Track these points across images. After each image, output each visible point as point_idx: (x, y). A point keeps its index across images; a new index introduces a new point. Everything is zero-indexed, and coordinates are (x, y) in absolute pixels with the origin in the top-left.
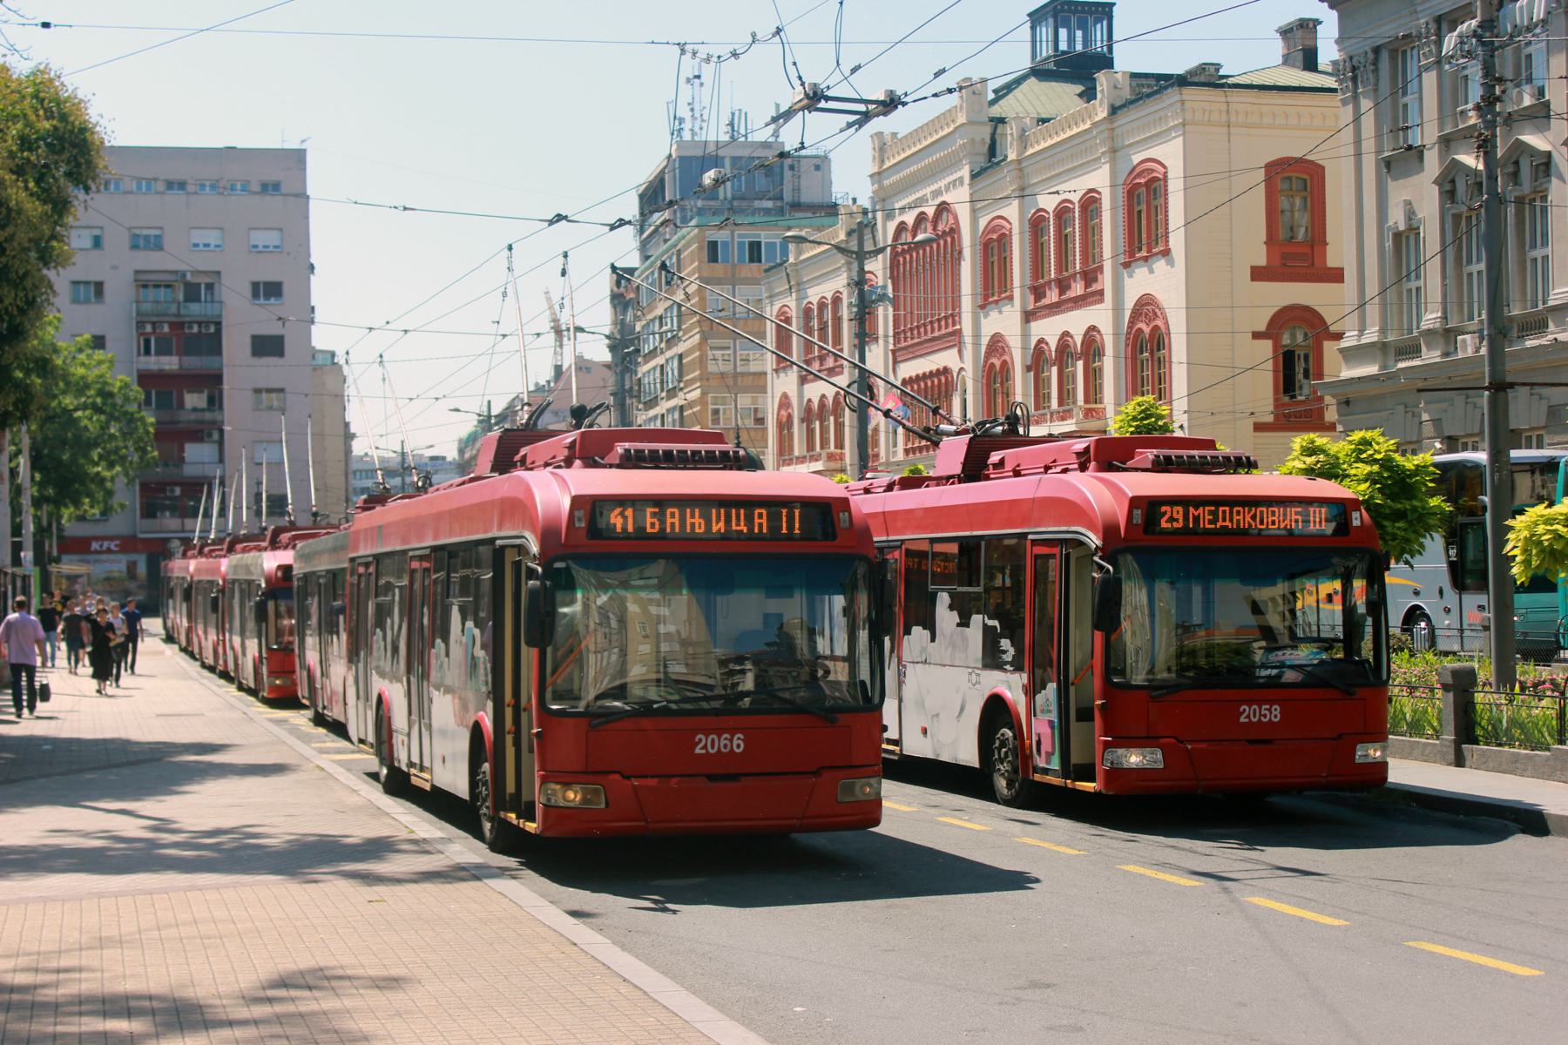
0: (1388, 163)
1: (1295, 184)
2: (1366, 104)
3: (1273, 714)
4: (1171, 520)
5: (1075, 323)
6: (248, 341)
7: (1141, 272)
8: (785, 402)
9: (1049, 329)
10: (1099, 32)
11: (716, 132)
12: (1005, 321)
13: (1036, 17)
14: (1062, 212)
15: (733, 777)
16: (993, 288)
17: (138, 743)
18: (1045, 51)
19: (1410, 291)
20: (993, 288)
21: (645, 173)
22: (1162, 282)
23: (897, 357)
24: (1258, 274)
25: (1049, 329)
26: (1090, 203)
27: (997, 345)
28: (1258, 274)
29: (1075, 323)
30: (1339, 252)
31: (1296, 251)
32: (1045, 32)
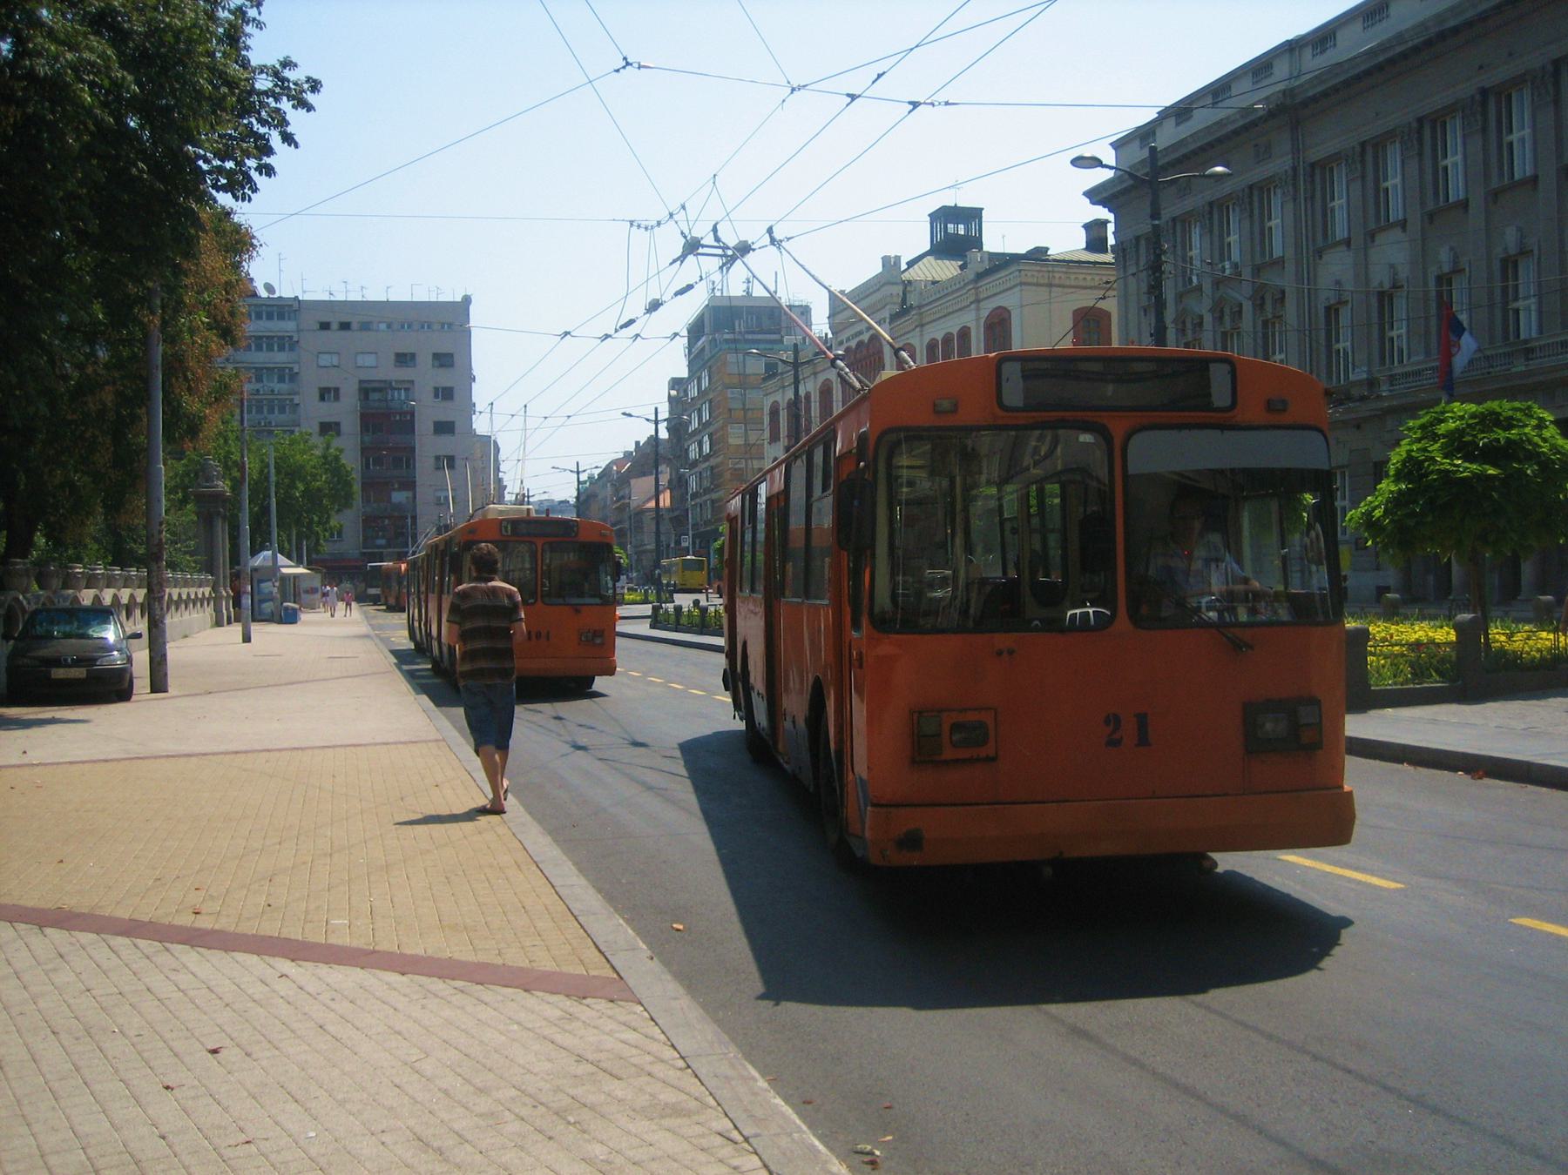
14: (948, 339)
26: (964, 333)
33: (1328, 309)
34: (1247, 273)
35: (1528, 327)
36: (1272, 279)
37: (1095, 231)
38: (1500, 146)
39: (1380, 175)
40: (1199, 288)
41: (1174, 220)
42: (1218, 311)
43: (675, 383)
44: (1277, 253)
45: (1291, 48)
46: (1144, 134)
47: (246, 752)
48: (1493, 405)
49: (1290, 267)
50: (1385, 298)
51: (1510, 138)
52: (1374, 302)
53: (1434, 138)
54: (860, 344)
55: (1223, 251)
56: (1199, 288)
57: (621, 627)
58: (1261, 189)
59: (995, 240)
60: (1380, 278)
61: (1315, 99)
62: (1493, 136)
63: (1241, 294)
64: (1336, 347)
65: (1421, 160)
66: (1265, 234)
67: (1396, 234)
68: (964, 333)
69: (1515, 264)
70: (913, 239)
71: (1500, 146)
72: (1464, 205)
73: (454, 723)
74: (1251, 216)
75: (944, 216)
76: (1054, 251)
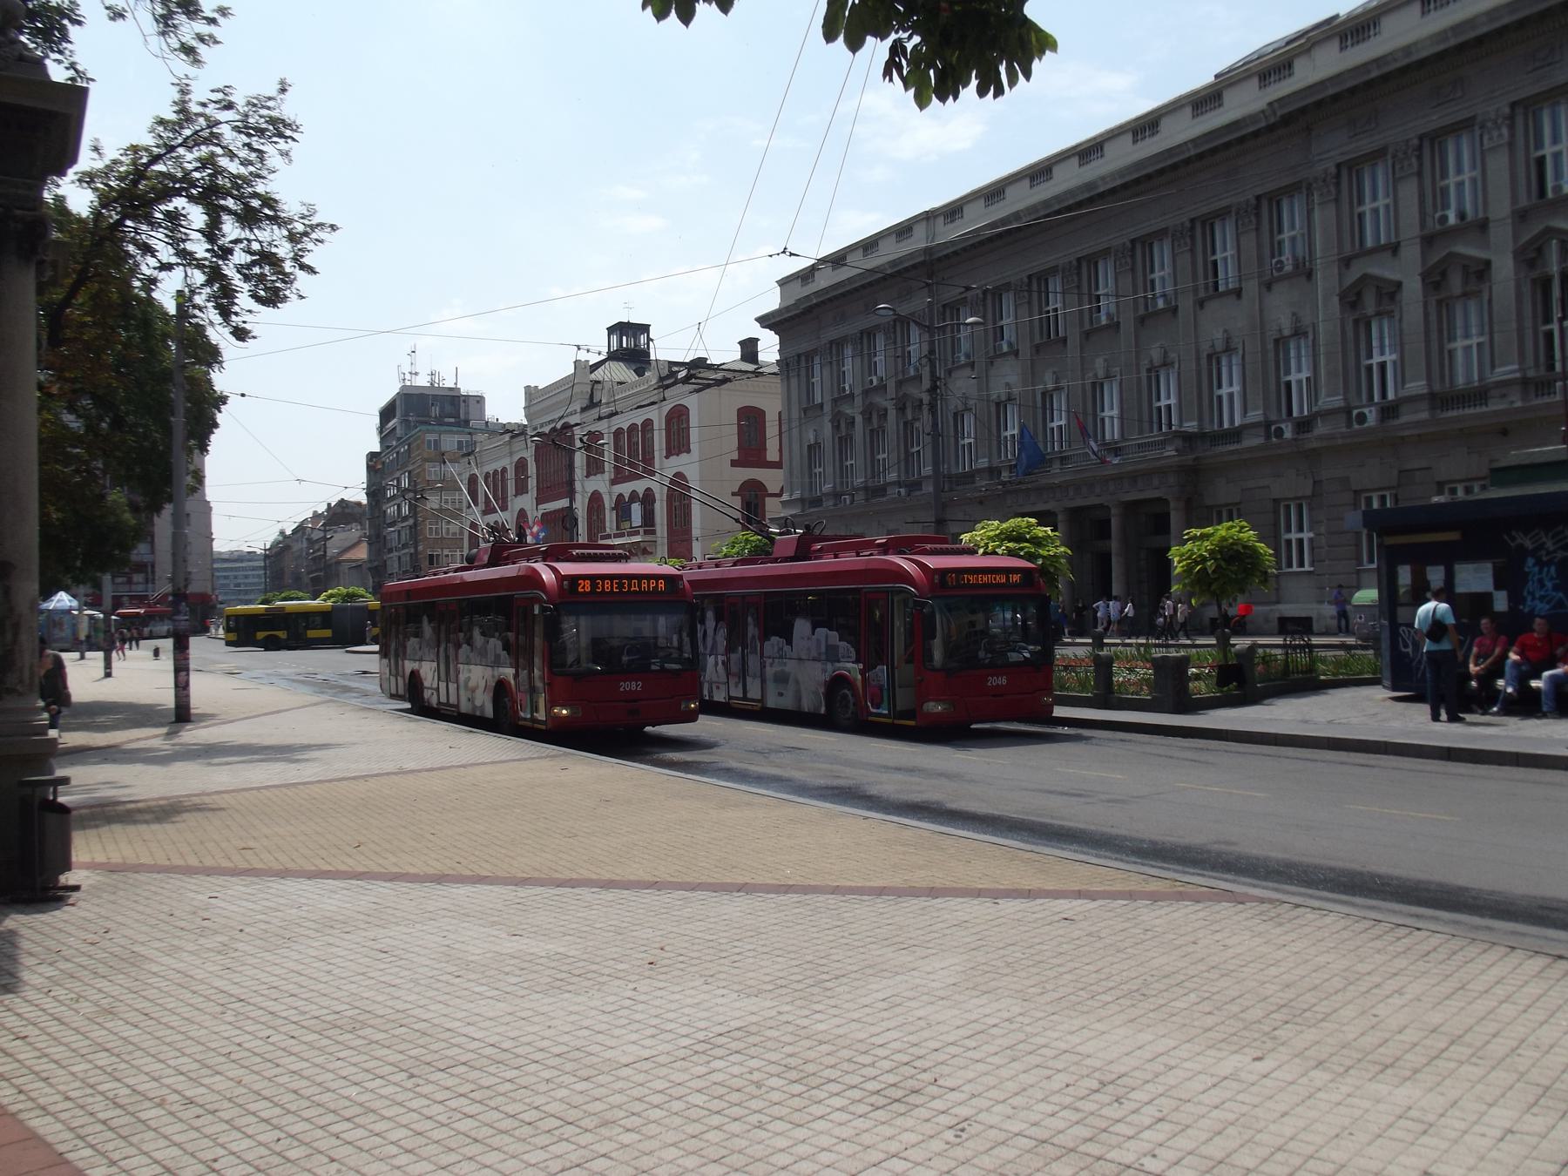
0: (805, 410)
1: (751, 420)
2: (794, 381)
3: (1003, 681)
4: (585, 586)
5: (640, 486)
6: (732, 12)
7: (519, 498)
8: (596, 498)
9: (625, 489)
10: (643, 339)
11: (422, 381)
12: (600, 483)
13: (611, 330)
14: (633, 427)
15: (1080, 795)
16: (594, 467)
17: (65, 687)
18: (615, 347)
19: (1159, 409)
20: (594, 467)
21: (384, 401)
22: (687, 464)
23: (539, 501)
24: (734, 463)
25: (625, 489)
26: (504, 470)
27: (522, 514)
28: (734, 463)
29: (640, 486)
30: (772, 455)
31: (751, 451)
32: (614, 338)
33: (955, 414)
34: (891, 385)
35: (1112, 432)
36: (879, 400)
37: (749, 348)
38: (1352, 214)
39: (840, 363)
40: (852, 395)
41: (831, 342)
42: (867, 414)
43: (372, 456)
44: (818, 400)
45: (928, 217)
46: (806, 275)
47: (1051, 792)
48: (1013, 522)
49: (858, 401)
50: (1000, 406)
51: (1361, 209)
52: (993, 409)
53: (1204, 234)
54: (554, 429)
55: (872, 368)
56: (852, 395)
57: (82, 783)
58: (1143, 243)
59: (667, 348)
60: (998, 391)
61: (947, 256)
62: (1266, 235)
63: (885, 402)
64: (1004, 434)
65: (1338, 209)
66: (841, 376)
67: (967, 371)
68: (648, 424)
69: (1102, 385)
70: (598, 345)
71: (1352, 214)
72: (821, 406)
73: (361, 847)
74: (1192, 251)
75: (620, 329)
76: (714, 359)
